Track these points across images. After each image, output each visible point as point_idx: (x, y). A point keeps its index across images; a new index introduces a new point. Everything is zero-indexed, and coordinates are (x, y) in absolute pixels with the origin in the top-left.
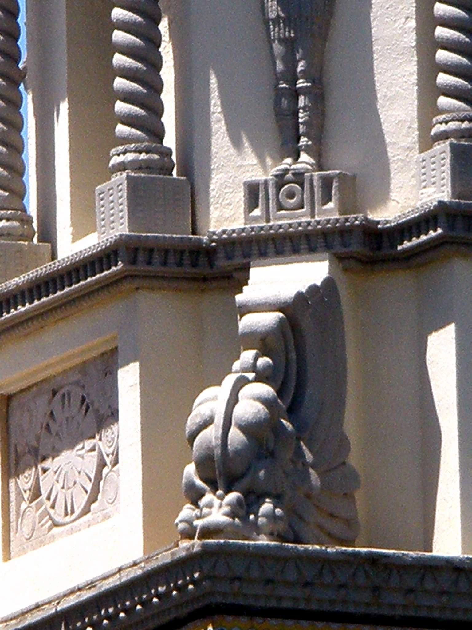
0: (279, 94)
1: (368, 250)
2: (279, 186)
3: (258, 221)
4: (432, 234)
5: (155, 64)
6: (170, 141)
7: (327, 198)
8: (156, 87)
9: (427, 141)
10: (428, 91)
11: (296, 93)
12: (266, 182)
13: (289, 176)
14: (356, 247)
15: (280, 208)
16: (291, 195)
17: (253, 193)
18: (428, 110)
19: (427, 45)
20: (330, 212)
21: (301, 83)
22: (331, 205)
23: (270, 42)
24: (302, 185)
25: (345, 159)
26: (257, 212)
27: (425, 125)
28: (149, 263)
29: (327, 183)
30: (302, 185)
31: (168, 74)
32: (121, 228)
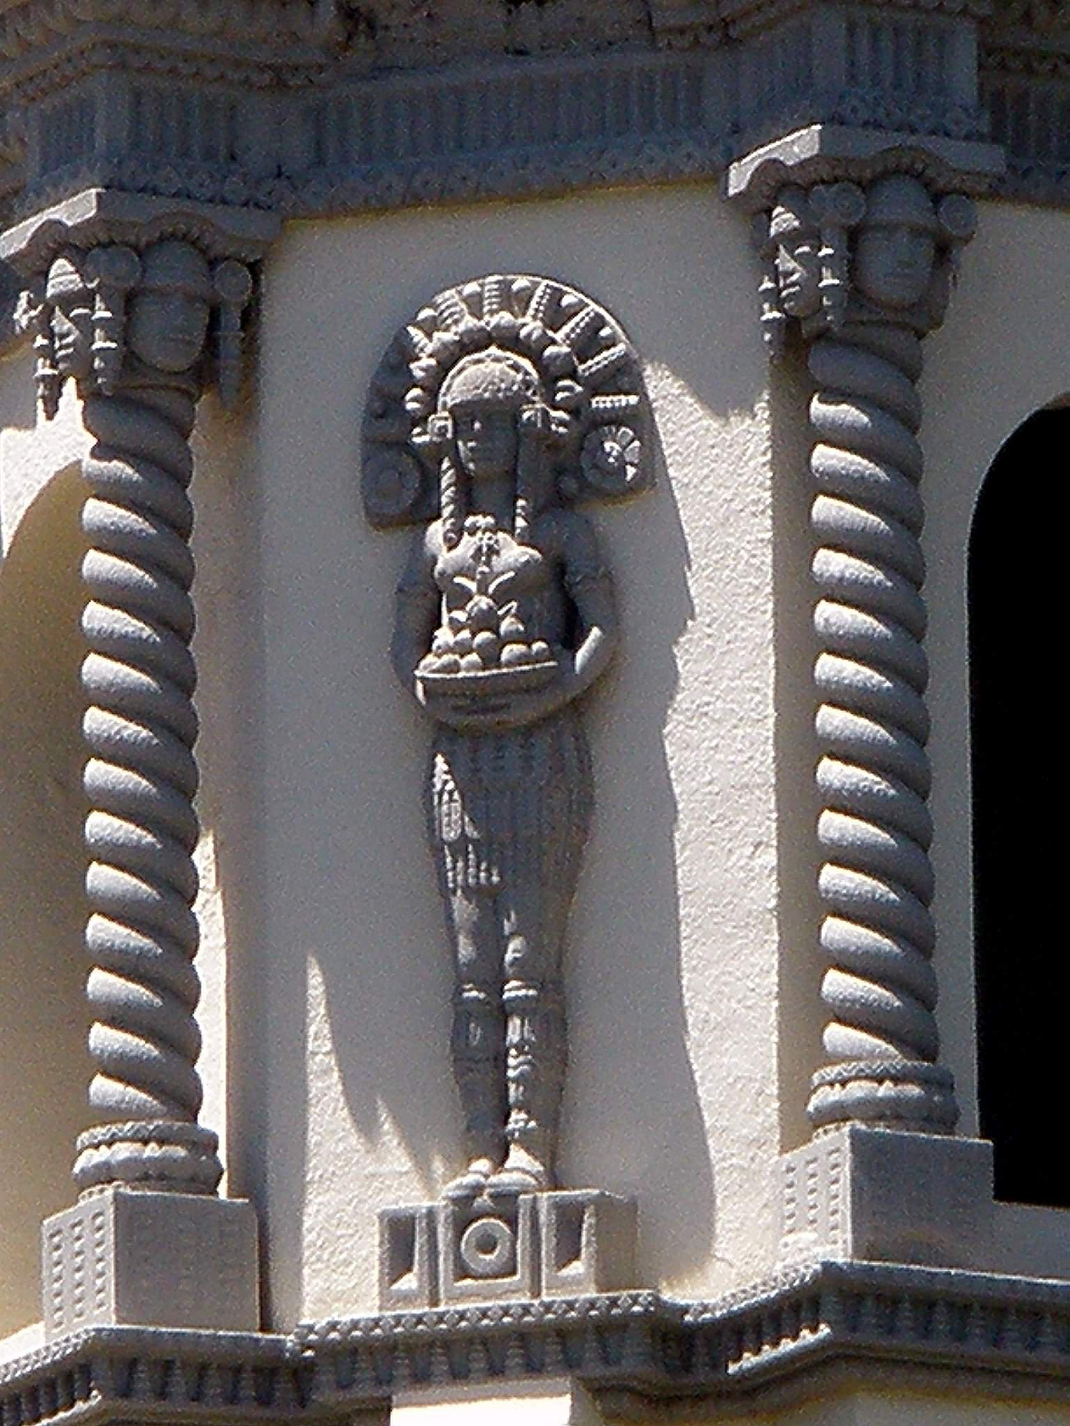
0: (463, 1013)
1: (708, 1354)
2: (461, 1224)
3: (410, 1302)
4: (807, 1337)
5: (183, 943)
6: (213, 1116)
7: (569, 1253)
8: (184, 995)
9: (799, 1125)
10: (804, 1012)
11: (501, 1013)
12: (431, 1214)
13: (484, 1200)
14: (634, 1363)
15: (463, 1272)
16: (487, 1245)
17: (401, 1238)
18: (801, 1053)
19: (802, 907)
20: (575, 1285)
21: (513, 990)
22: (577, 1268)
23: (446, 894)
24: (512, 1222)
25: (612, 1163)
26: (409, 1282)
27: (794, 1087)
28: (197, 1397)
29: (569, 1218)
30: (512, 1222)
31: (211, 964)
32: (99, 1314)
